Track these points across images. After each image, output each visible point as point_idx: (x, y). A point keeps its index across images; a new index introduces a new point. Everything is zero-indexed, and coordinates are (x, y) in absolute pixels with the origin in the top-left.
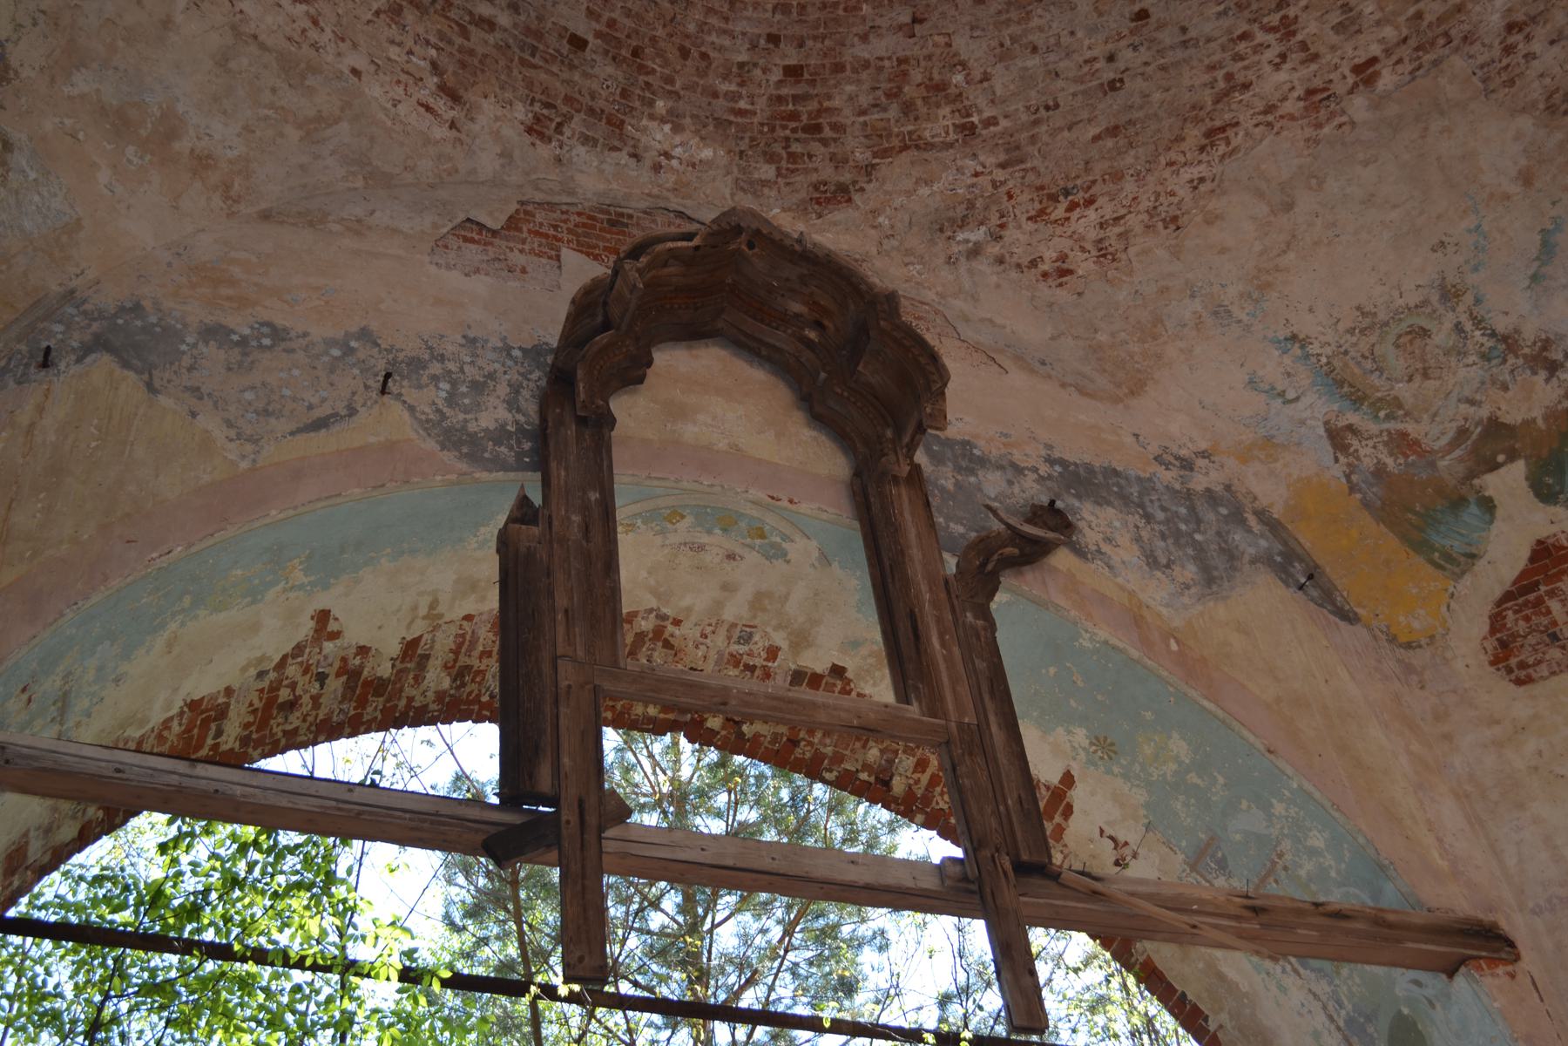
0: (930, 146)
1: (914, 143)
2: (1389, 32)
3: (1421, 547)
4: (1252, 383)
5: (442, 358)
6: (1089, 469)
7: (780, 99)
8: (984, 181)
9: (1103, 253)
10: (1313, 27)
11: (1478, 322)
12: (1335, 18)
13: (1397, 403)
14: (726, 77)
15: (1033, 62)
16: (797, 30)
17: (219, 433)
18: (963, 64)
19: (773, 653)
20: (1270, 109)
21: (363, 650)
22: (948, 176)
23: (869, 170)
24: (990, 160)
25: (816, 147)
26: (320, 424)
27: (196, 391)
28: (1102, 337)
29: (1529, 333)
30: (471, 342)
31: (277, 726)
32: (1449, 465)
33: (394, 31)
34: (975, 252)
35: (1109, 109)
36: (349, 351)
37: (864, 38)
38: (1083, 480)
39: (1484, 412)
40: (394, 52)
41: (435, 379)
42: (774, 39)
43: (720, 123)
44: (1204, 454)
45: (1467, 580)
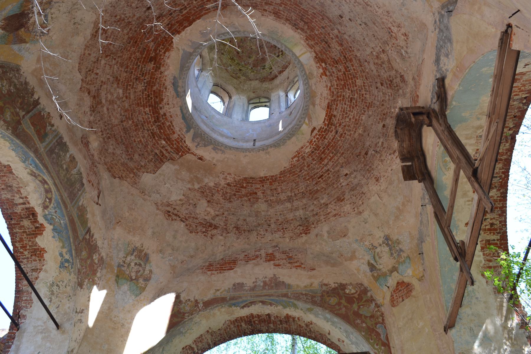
1: (389, 61)
7: (387, 87)
8: (392, 49)
15: (367, 39)
16: (374, 83)
18: (372, 52)
22: (394, 56)
23: (397, 71)
25: (394, 81)
33: (385, 161)
34: (406, 52)
35: (370, 24)
37: (372, 71)
40: (388, 162)
42: (377, 88)
43: (394, 99)
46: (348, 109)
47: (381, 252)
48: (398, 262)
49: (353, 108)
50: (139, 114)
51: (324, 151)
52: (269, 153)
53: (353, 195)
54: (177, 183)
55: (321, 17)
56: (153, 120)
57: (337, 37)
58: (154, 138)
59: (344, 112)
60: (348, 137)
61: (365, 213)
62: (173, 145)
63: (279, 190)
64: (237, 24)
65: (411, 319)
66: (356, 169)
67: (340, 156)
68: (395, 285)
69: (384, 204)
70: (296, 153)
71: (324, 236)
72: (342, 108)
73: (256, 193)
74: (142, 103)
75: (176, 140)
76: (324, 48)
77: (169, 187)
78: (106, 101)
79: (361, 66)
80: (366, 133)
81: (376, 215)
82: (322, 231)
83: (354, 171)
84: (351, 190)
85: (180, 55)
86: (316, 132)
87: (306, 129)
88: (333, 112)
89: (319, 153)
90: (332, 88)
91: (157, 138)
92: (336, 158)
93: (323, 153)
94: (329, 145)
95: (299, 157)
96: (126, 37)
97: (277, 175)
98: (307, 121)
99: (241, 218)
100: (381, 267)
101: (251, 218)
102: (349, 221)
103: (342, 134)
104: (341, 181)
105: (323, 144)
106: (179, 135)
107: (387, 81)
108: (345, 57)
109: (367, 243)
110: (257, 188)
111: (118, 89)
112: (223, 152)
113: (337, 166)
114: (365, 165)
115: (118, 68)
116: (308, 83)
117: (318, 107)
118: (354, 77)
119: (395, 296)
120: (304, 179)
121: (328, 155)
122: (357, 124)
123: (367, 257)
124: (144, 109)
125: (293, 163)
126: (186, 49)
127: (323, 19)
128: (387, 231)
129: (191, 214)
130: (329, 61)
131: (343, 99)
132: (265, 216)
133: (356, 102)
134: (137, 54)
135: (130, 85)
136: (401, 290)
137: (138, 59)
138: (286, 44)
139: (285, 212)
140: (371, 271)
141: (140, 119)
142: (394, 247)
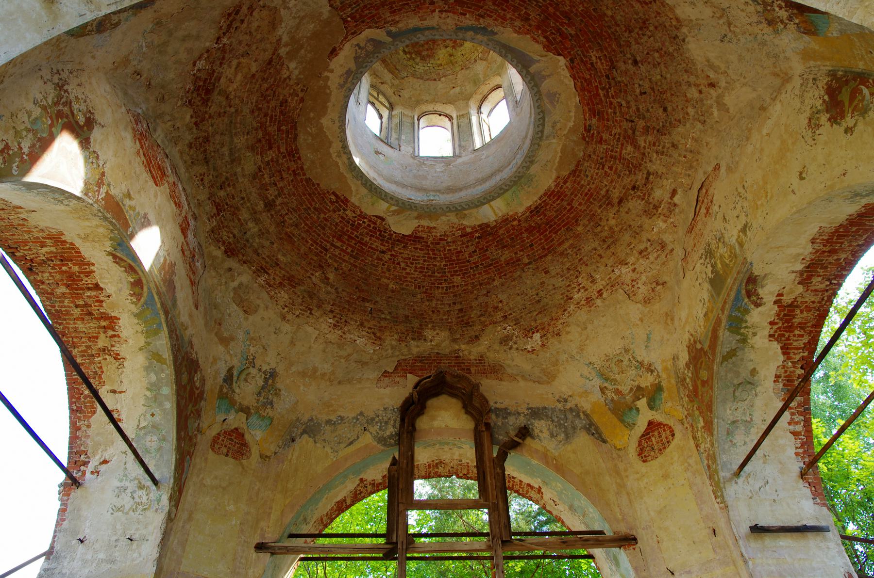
0: (496, 323)
6: (538, 408)
11: (634, 358)
13: (616, 380)
14: (444, 315)
20: (578, 303)
26: (351, 443)
29: (646, 362)
30: (385, 409)
31: (359, 497)
32: (629, 398)
36: (358, 419)
38: (536, 413)
39: (636, 384)
44: (570, 396)
45: (633, 431)
47: (253, 377)
48: (257, 410)
49: (420, 272)
51: (353, 238)
53: (304, 297)
54: (294, 18)
57: (519, 260)
65: (224, 489)
66: (340, 290)
67: (351, 264)
68: (233, 428)
69: (310, 348)
71: (233, 281)
73: (270, 148)
76: (502, 240)
79: (481, 284)
80: (390, 294)
81: (292, 343)
82: (239, 275)
83: (336, 289)
84: (309, 292)
85: (531, 54)
90: (445, 242)
92: (346, 258)
93: (350, 237)
94: (362, 244)
95: (337, 202)
96: (609, 13)
97: (304, 174)
98: (394, 208)
100: (237, 391)
103: (381, 260)
107: (466, 317)
108: (491, 265)
110: (279, 148)
112: (341, 86)
113: (336, 261)
114: (348, 301)
116: (450, 211)
118: (464, 274)
119: (221, 438)
120: (306, 217)
121: (349, 245)
123: (235, 362)
126: (538, 65)
127: (544, 249)
128: (280, 369)
129: (230, 51)
130: (483, 243)
131: (430, 258)
133: (429, 276)
136: (232, 440)
138: (510, 192)
139: (249, 204)
140: (225, 381)
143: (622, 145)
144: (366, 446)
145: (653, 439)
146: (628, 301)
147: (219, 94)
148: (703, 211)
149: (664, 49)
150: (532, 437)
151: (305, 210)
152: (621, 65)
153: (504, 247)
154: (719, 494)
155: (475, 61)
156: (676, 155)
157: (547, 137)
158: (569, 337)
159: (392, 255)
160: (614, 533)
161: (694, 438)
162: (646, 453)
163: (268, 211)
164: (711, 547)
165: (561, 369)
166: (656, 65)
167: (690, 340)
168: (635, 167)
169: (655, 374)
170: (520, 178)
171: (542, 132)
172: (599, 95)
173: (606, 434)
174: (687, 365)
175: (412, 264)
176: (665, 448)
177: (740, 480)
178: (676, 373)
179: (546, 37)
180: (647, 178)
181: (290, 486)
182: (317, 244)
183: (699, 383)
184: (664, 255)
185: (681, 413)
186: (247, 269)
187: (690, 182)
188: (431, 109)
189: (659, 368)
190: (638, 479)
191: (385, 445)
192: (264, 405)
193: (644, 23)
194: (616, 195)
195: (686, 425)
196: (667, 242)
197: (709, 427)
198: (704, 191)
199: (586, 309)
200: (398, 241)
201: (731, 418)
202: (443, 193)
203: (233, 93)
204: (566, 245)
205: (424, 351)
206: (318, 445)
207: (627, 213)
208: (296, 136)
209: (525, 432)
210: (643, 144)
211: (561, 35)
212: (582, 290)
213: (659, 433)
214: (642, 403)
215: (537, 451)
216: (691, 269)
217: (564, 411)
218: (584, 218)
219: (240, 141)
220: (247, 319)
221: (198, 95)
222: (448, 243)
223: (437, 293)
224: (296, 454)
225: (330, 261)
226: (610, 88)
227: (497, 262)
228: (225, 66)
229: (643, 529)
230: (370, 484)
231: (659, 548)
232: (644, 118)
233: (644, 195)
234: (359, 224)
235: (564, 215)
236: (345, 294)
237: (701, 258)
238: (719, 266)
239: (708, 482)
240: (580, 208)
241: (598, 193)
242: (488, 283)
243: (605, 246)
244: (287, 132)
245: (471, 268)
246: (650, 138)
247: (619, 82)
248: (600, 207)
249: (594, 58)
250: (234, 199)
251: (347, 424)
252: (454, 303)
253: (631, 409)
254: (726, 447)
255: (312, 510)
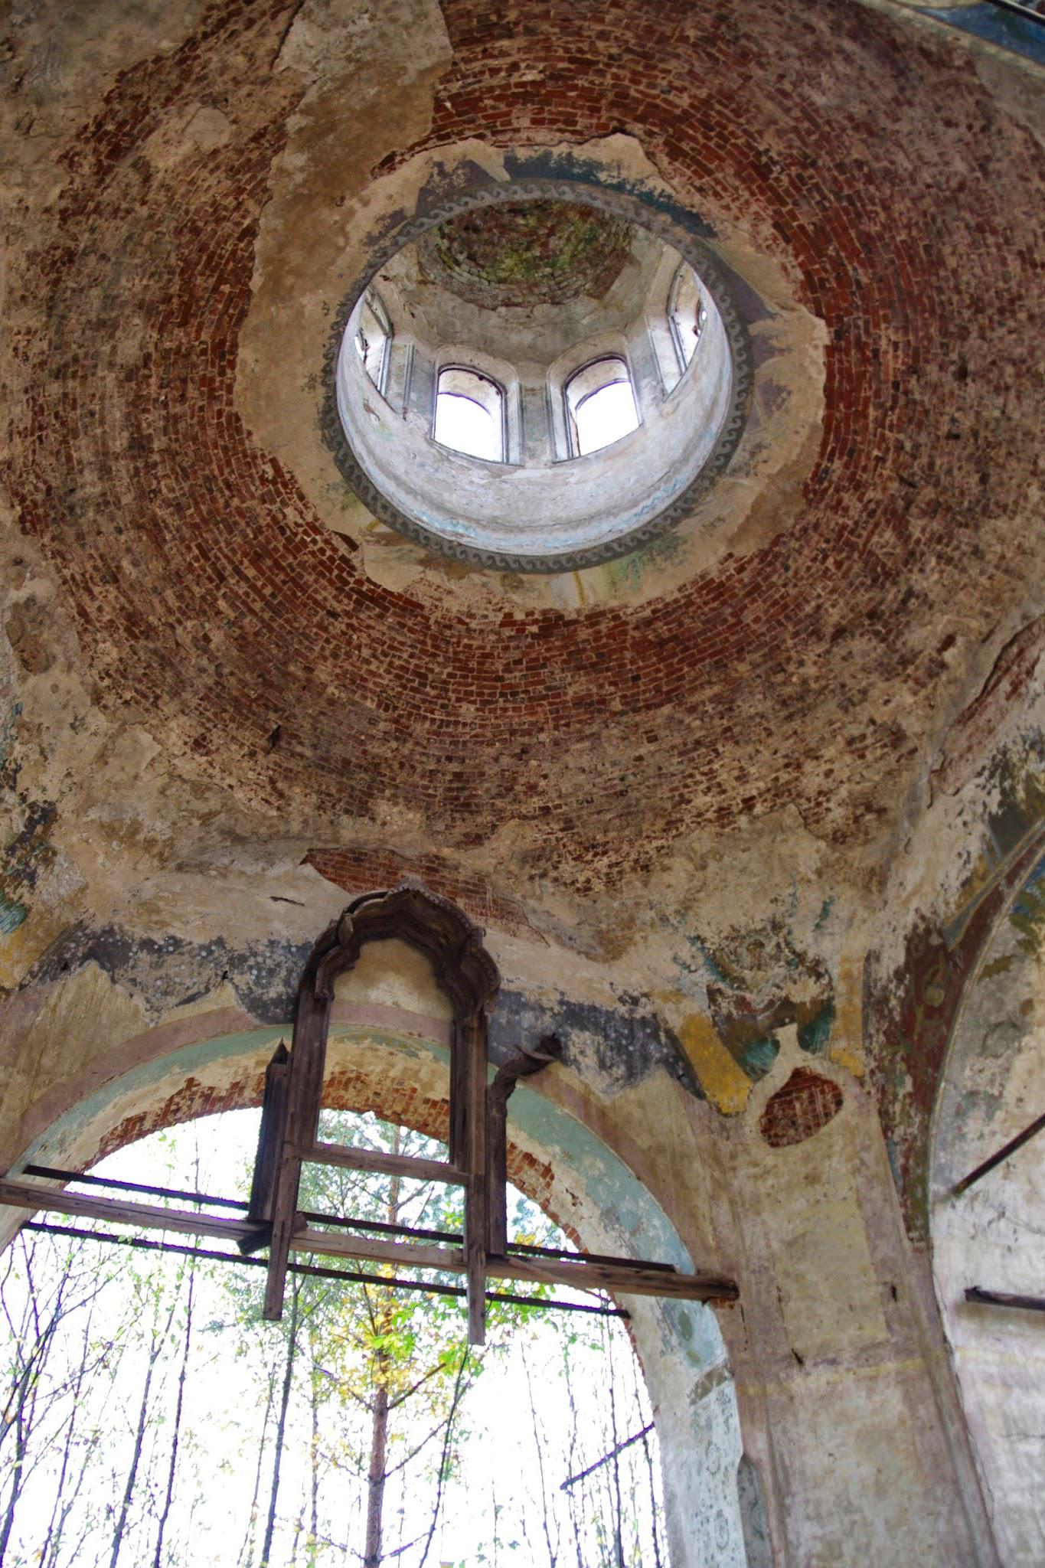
2: (761, 785)
3: (741, 1061)
4: (675, 959)
5: (255, 955)
6: (581, 1006)
7: (450, 790)
9: (610, 882)
10: (725, 776)
11: (788, 944)
12: (736, 773)
13: (743, 981)
14: (422, 777)
17: (142, 1006)
19: (414, 1090)
20: (700, 815)
21: (211, 1089)
24: (556, 827)
26: (191, 999)
27: (133, 981)
28: (603, 926)
29: (811, 955)
30: (272, 943)
36: (210, 952)
38: (578, 1015)
40: (251, 775)
41: (251, 968)
44: (645, 995)
45: (759, 1084)
46: (397, 662)
49: (398, 677)
50: (691, 73)
51: (282, 569)
52: (312, 387)
53: (149, 666)
54: (349, 59)
55: (665, 689)
56: (633, 93)
58: (571, 60)
59: (391, 647)
60: (317, 649)
61: (101, 717)
62: (497, 98)
63: (176, 409)
64: (745, 482)
67: (262, 620)
69: (136, 777)
70: (288, 476)
71: (17, 588)
72: (402, 644)
73: (183, 323)
74: (718, 107)
75: (508, 114)
77: (352, 28)
78: (840, 50)
79: (513, 733)
81: (102, 758)
82: (33, 578)
84: (162, 658)
86: (343, 549)
87: (359, 520)
88: (395, 614)
89: (276, 549)
91: (561, 65)
92: (258, 606)
93: (276, 563)
94: (297, 585)
96: (952, 262)
97: (230, 403)
98: (383, 529)
99: (108, 267)
101: (96, 304)
102: (70, 667)
104: (189, 624)
105: (304, 568)
106: (517, 130)
107: (466, 793)
108: (545, 697)
109: (18, 749)
111: (836, 102)
112: (371, 240)
113: (232, 606)
114: (236, 700)
115: (892, 162)
116: (493, 566)
117: (415, 572)
118: (484, 703)
120: (202, 496)
122: (353, 682)
124: (693, 97)
125: (259, 461)
126: (769, 322)
127: (658, 690)
129: (199, 80)
130: (540, 649)
131: (424, 652)
132: (96, 355)
133: (413, 689)
134: (878, 228)
135: (809, 133)
137: (859, 216)
138: (625, 560)
141: (673, 65)
142: (33, 849)
143: (876, 525)
144: (224, 1012)
145: (797, 1105)
146: (801, 831)
147: (134, 165)
148: (1005, 686)
149: (1030, 362)
150: (565, 1062)
151: (207, 479)
152: (932, 371)
153: (578, 668)
154: (919, 1223)
155: (576, 293)
156: (974, 572)
157: (735, 471)
158: (667, 878)
159: (350, 626)
160: (699, 1272)
161: (883, 1113)
162: (779, 1131)
163: (134, 458)
164: (882, 1319)
165: (637, 937)
166: (1000, 389)
167: (915, 927)
168: (887, 574)
169: (825, 981)
170: (654, 537)
171: (728, 457)
172: (866, 417)
173: (705, 1079)
174: (899, 975)
175: (385, 655)
176: (818, 1125)
177: (961, 1204)
178: (867, 987)
179: (808, 274)
180: (904, 602)
181: (47, 1062)
182: (207, 559)
183: (920, 1011)
184: (893, 757)
185: (861, 1062)
186: (52, 569)
187: (985, 630)
188: (466, 360)
189: (835, 972)
190: (756, 1177)
191: (263, 1017)
192: (17, 876)
193: (1012, 301)
194: (834, 616)
195: (868, 1087)
196: (908, 733)
197: (925, 1096)
198: (1015, 650)
199: (714, 829)
200: (372, 599)
201: (969, 1084)
202: (484, 527)
203: (160, 175)
204: (709, 692)
205: (366, 842)
206: (119, 988)
207: (844, 659)
208: (243, 314)
209: (553, 1046)
210: (917, 534)
211: (838, 279)
212: (715, 790)
213: (811, 1096)
214: (788, 1034)
215: (570, 1090)
216: (951, 790)
217: (629, 1022)
218: (756, 650)
219: (132, 285)
220: (23, 679)
221: (95, 150)
222: (469, 630)
223: (420, 729)
224: (69, 997)
225: (222, 604)
226: (892, 408)
227: (558, 696)
228: (173, 109)
229: (753, 1272)
230: (203, 1095)
231: (781, 1311)
232: (937, 484)
233: (889, 632)
234: (303, 541)
235: (719, 634)
236: (233, 680)
237: (979, 774)
238: (1021, 794)
239: (896, 1198)
240: (754, 627)
241: (798, 606)
242: (528, 733)
243: (783, 714)
244: (230, 299)
245: (502, 695)
246: (936, 526)
247: (915, 402)
248: (796, 634)
249: (884, 343)
250: (74, 408)
251: (186, 958)
252: (449, 759)
253: (763, 1041)
254: (950, 1137)
255: (80, 1126)
